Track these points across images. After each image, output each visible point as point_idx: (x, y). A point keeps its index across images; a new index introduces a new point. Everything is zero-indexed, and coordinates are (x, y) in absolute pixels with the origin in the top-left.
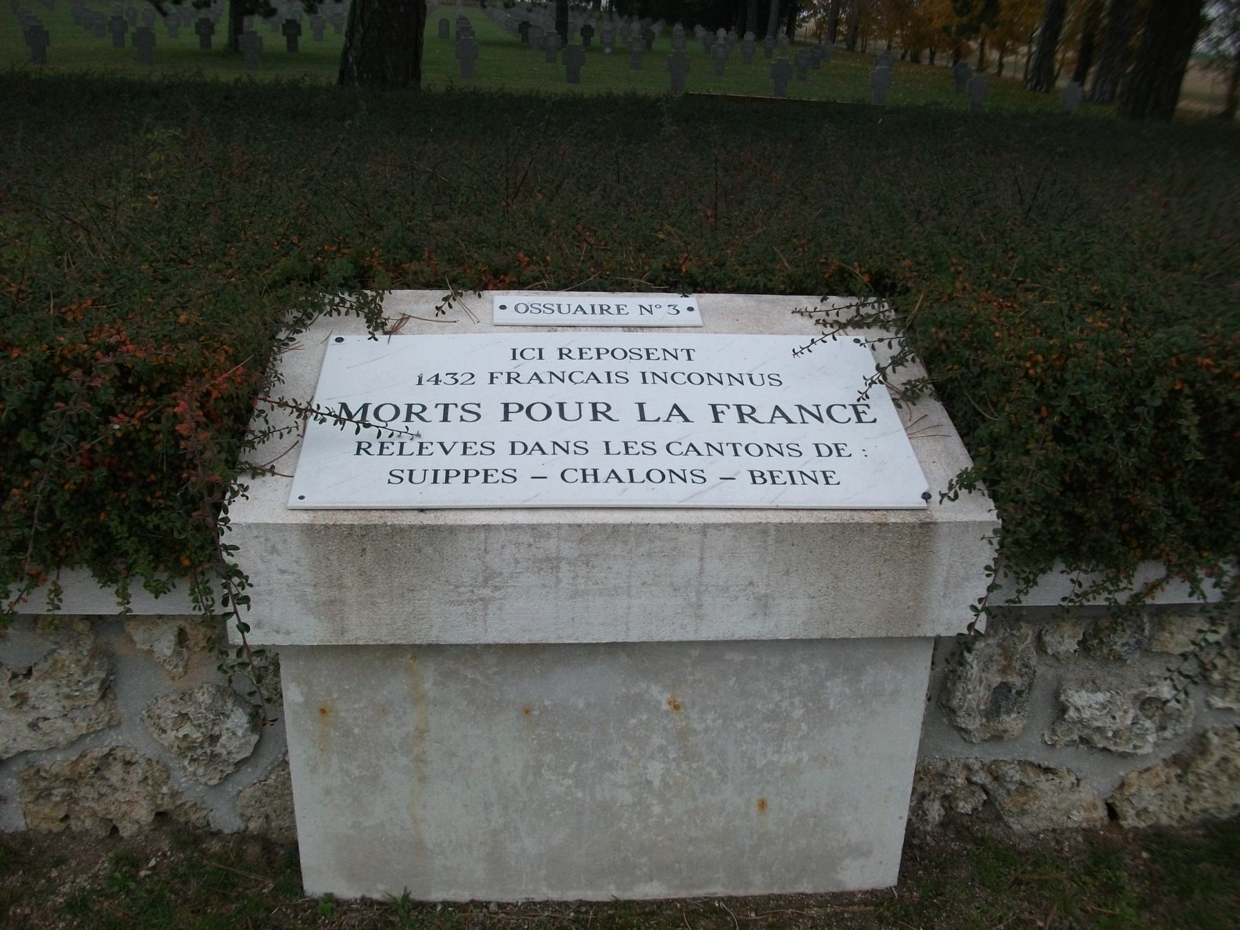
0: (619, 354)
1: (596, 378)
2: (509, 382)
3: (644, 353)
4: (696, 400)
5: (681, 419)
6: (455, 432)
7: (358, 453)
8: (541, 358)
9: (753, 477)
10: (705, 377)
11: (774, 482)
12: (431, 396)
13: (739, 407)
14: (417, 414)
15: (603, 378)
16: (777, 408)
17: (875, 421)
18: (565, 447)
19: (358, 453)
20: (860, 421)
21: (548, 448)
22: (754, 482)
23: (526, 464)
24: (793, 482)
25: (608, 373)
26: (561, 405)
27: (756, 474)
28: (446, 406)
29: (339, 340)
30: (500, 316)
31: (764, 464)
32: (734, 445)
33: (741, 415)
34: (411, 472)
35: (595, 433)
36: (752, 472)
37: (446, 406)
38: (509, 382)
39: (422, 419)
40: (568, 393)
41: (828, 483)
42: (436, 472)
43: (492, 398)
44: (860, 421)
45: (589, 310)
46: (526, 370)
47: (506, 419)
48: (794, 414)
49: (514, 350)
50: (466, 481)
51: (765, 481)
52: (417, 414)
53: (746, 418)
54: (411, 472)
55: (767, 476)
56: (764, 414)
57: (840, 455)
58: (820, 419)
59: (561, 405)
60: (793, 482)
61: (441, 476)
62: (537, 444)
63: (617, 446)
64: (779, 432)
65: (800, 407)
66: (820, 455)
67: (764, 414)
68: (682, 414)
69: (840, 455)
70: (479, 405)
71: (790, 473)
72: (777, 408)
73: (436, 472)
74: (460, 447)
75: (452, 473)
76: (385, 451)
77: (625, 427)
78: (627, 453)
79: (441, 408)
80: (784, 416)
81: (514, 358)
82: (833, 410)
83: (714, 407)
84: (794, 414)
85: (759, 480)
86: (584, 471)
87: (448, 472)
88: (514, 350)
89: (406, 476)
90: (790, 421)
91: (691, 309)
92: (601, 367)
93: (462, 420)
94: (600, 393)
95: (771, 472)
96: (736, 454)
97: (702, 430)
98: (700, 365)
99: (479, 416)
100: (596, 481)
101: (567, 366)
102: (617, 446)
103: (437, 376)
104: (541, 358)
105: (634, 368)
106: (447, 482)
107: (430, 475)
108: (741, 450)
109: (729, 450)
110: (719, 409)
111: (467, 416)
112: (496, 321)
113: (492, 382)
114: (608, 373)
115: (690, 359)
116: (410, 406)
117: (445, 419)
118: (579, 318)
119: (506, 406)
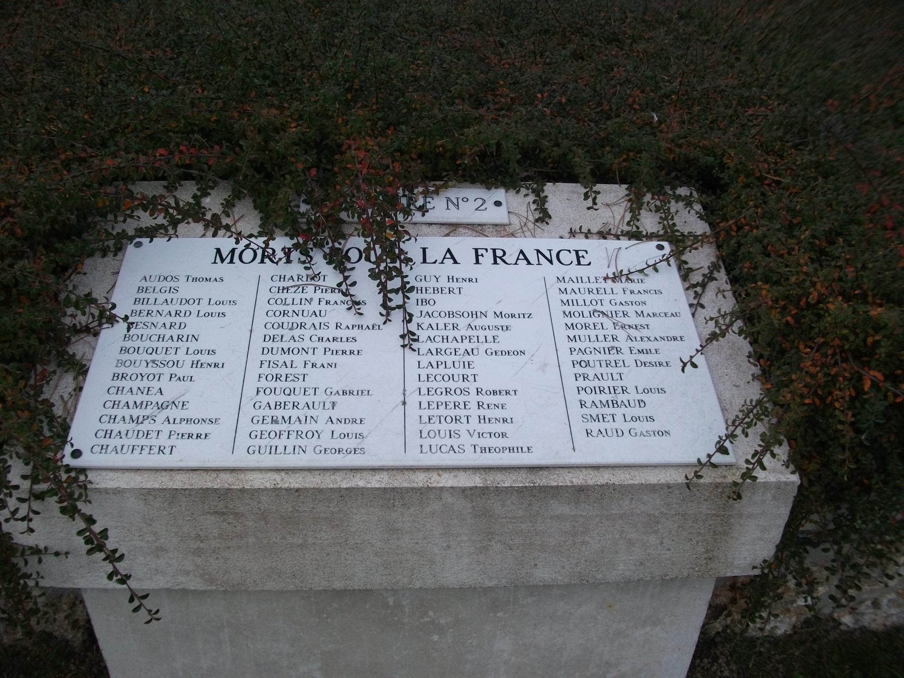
14: (500, 258)
17: (589, 264)
33: (495, 256)
52: (500, 258)
53: (499, 260)
58: (551, 262)
65: (538, 251)
68: (453, 257)
91: (498, 204)
113: (477, 262)
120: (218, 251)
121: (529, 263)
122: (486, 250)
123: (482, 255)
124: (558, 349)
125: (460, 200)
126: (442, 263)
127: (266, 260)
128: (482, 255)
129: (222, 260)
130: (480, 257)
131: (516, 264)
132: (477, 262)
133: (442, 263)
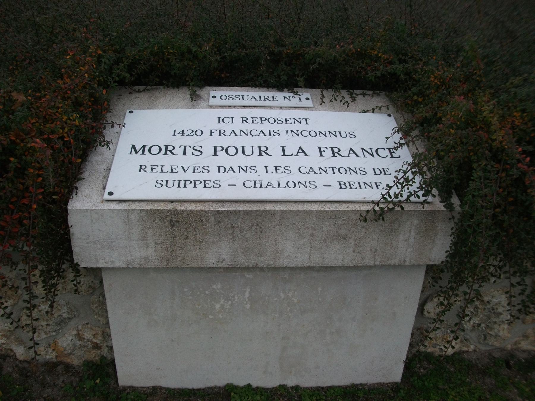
0: (272, 121)
1: (263, 133)
2: (220, 135)
3: (284, 120)
4: (311, 145)
5: (303, 154)
6: (190, 160)
7: (140, 171)
8: (232, 122)
9: (340, 185)
10: (318, 133)
11: (351, 188)
12: (178, 141)
13: (332, 148)
14: (170, 151)
15: (267, 133)
16: (300, 148)
17: (399, 157)
18: (245, 169)
19: (140, 171)
20: (392, 157)
21: (236, 169)
22: (341, 188)
23: (226, 178)
24: (361, 188)
25: (270, 131)
26: (243, 147)
27: (342, 183)
28: (185, 147)
29: (131, 112)
30: (213, 102)
31: (346, 178)
32: (333, 168)
33: (333, 152)
34: (167, 181)
35: (260, 162)
36: (339, 182)
37: (185, 147)
38: (220, 135)
39: (173, 153)
40: (247, 141)
41: (378, 188)
42: (180, 181)
43: (208, 143)
44: (392, 157)
45: (258, 98)
46: (228, 128)
47: (215, 154)
48: (359, 152)
49: (219, 118)
50: (195, 186)
51: (346, 187)
52: (170, 151)
53: (336, 154)
54: (167, 181)
55: (347, 185)
56: (344, 153)
57: (385, 174)
58: (373, 155)
59: (243, 147)
60: (361, 188)
61: (182, 183)
62: (231, 167)
63: (271, 169)
64: (353, 162)
65: (363, 149)
66: (376, 174)
67: (344, 153)
68: (304, 152)
69: (385, 174)
70: (201, 147)
71: (359, 183)
72: (300, 148)
73: (180, 181)
74: (192, 169)
75: (188, 182)
76: (154, 170)
77: (275, 159)
78: (276, 172)
79: (182, 148)
80: (355, 153)
81: (219, 122)
82: (379, 150)
83: (320, 148)
84: (359, 152)
85: (343, 187)
86: (255, 182)
87: (185, 181)
88: (219, 118)
89: (164, 183)
90: (357, 156)
91: (308, 99)
92: (266, 127)
93: (193, 154)
94: (262, 141)
95: (349, 183)
96: (334, 173)
97: (314, 160)
98: (312, 126)
99: (201, 153)
100: (261, 187)
101: (245, 127)
102: (271, 169)
103: (183, 131)
104: (232, 122)
105: (281, 127)
106: (185, 186)
107: (177, 183)
108: (336, 171)
109: (330, 171)
110: (322, 149)
111: (196, 153)
112: (210, 104)
113: (211, 135)
114: (270, 131)
115: (307, 123)
116: (167, 147)
117: (185, 154)
118: (253, 103)
119: (215, 148)
120: (133, 146)
121: (357, 156)
122: (326, 148)
123: (324, 151)
124: (315, 153)
125: (327, 168)
126: (297, 155)
127: (168, 153)
128: (324, 151)
129: (136, 152)
130: (393, 154)
131: (348, 156)
132: (211, 135)
133: (297, 155)
